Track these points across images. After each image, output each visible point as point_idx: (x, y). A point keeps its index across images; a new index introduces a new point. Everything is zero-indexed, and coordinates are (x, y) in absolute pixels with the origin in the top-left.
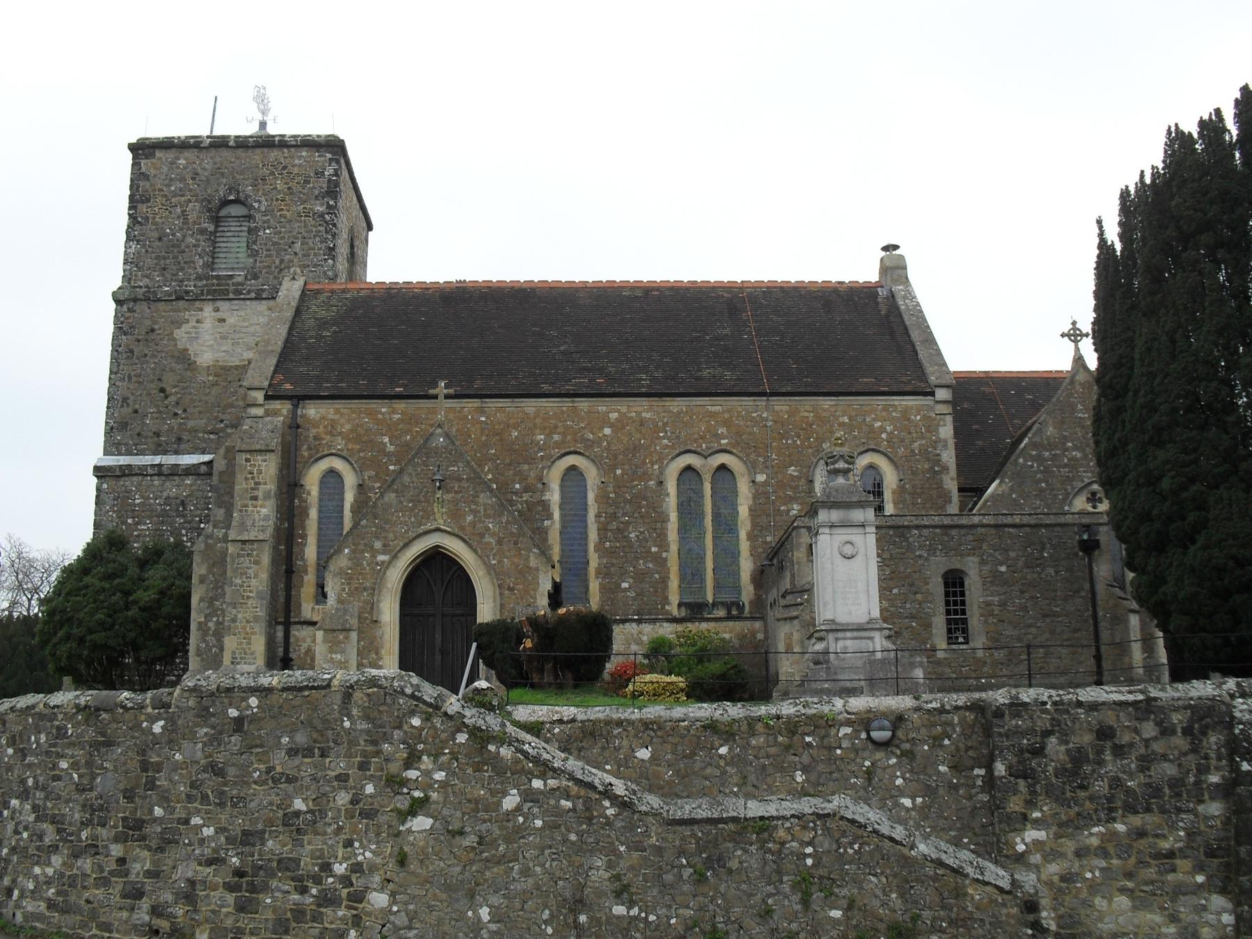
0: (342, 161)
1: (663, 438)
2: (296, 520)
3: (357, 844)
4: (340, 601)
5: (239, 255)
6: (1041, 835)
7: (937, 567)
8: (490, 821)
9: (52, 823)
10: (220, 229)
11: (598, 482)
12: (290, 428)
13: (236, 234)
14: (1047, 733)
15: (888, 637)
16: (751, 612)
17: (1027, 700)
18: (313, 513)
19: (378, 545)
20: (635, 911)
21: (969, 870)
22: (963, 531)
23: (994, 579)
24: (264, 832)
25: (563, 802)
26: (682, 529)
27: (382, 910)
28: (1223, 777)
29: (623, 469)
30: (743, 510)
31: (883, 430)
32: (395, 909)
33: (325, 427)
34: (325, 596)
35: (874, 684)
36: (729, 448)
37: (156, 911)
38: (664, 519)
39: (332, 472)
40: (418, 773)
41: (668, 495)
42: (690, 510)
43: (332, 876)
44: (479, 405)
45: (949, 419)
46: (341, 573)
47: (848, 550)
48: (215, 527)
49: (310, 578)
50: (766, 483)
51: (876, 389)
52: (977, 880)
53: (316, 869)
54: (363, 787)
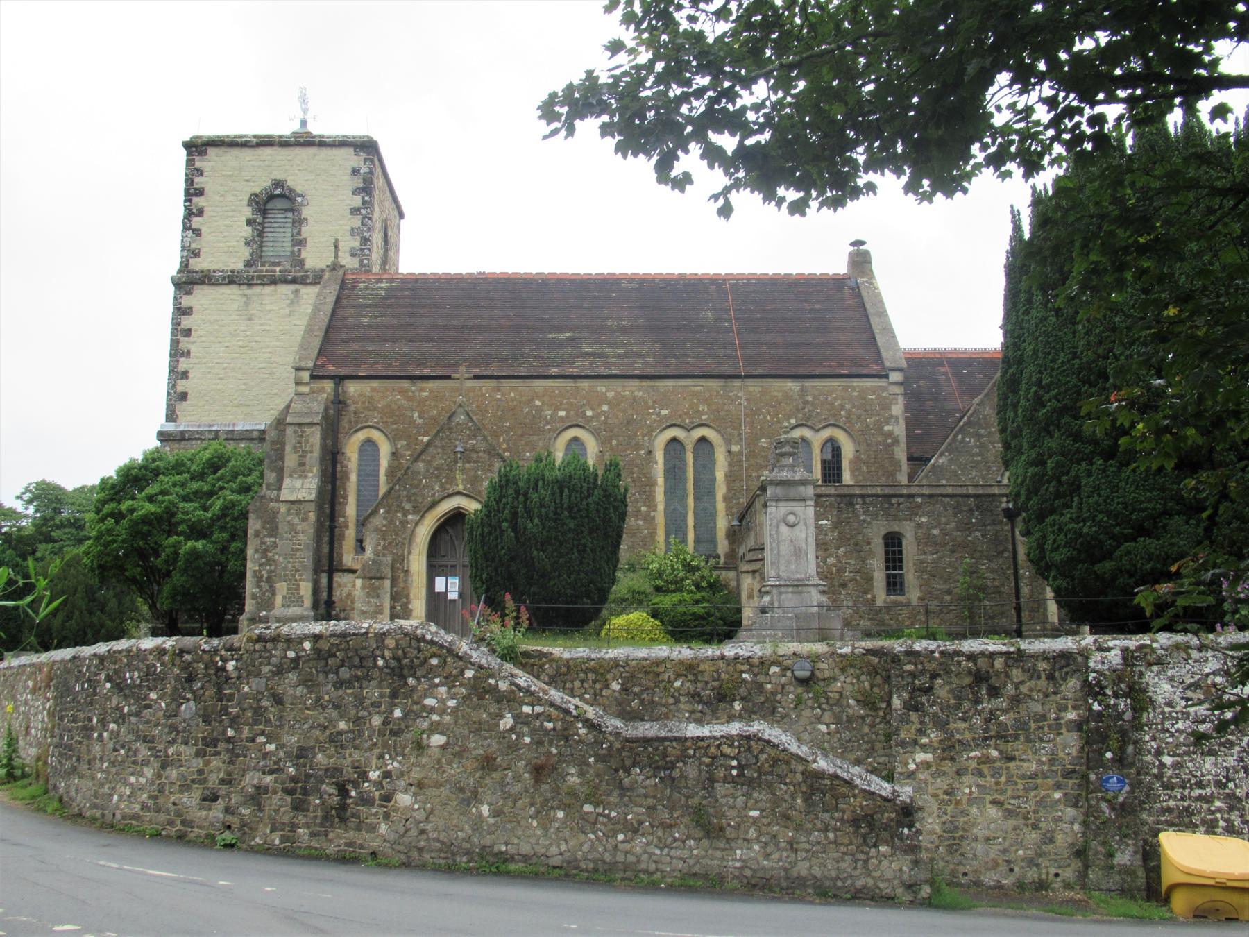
0: (376, 160)
1: (652, 414)
2: (338, 483)
3: (387, 756)
4: (376, 553)
5: (285, 244)
6: (929, 757)
7: (876, 533)
8: (491, 737)
9: (145, 741)
10: (267, 220)
11: (596, 450)
12: (332, 402)
13: (282, 225)
14: (934, 676)
15: (823, 592)
16: (725, 563)
17: (920, 649)
18: (353, 477)
19: (408, 506)
20: (600, 810)
21: (858, 781)
22: (901, 500)
23: (926, 541)
24: (314, 748)
25: (546, 724)
26: (668, 492)
27: (406, 808)
28: (1078, 715)
29: (618, 440)
30: (720, 476)
31: (842, 407)
32: (416, 806)
33: (363, 403)
34: (363, 550)
35: (800, 633)
36: (708, 423)
37: (227, 810)
38: (652, 483)
39: (369, 442)
40: (435, 701)
41: (656, 463)
42: (674, 472)
43: (368, 781)
44: (495, 385)
45: (900, 399)
46: (377, 530)
47: (791, 518)
48: (268, 488)
49: (350, 534)
50: (740, 453)
51: (837, 372)
52: (865, 790)
53: (356, 776)
54: (392, 712)
